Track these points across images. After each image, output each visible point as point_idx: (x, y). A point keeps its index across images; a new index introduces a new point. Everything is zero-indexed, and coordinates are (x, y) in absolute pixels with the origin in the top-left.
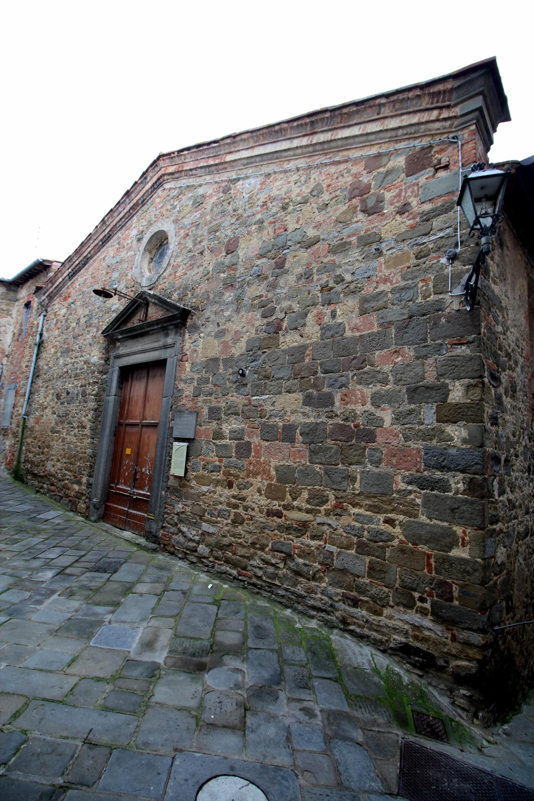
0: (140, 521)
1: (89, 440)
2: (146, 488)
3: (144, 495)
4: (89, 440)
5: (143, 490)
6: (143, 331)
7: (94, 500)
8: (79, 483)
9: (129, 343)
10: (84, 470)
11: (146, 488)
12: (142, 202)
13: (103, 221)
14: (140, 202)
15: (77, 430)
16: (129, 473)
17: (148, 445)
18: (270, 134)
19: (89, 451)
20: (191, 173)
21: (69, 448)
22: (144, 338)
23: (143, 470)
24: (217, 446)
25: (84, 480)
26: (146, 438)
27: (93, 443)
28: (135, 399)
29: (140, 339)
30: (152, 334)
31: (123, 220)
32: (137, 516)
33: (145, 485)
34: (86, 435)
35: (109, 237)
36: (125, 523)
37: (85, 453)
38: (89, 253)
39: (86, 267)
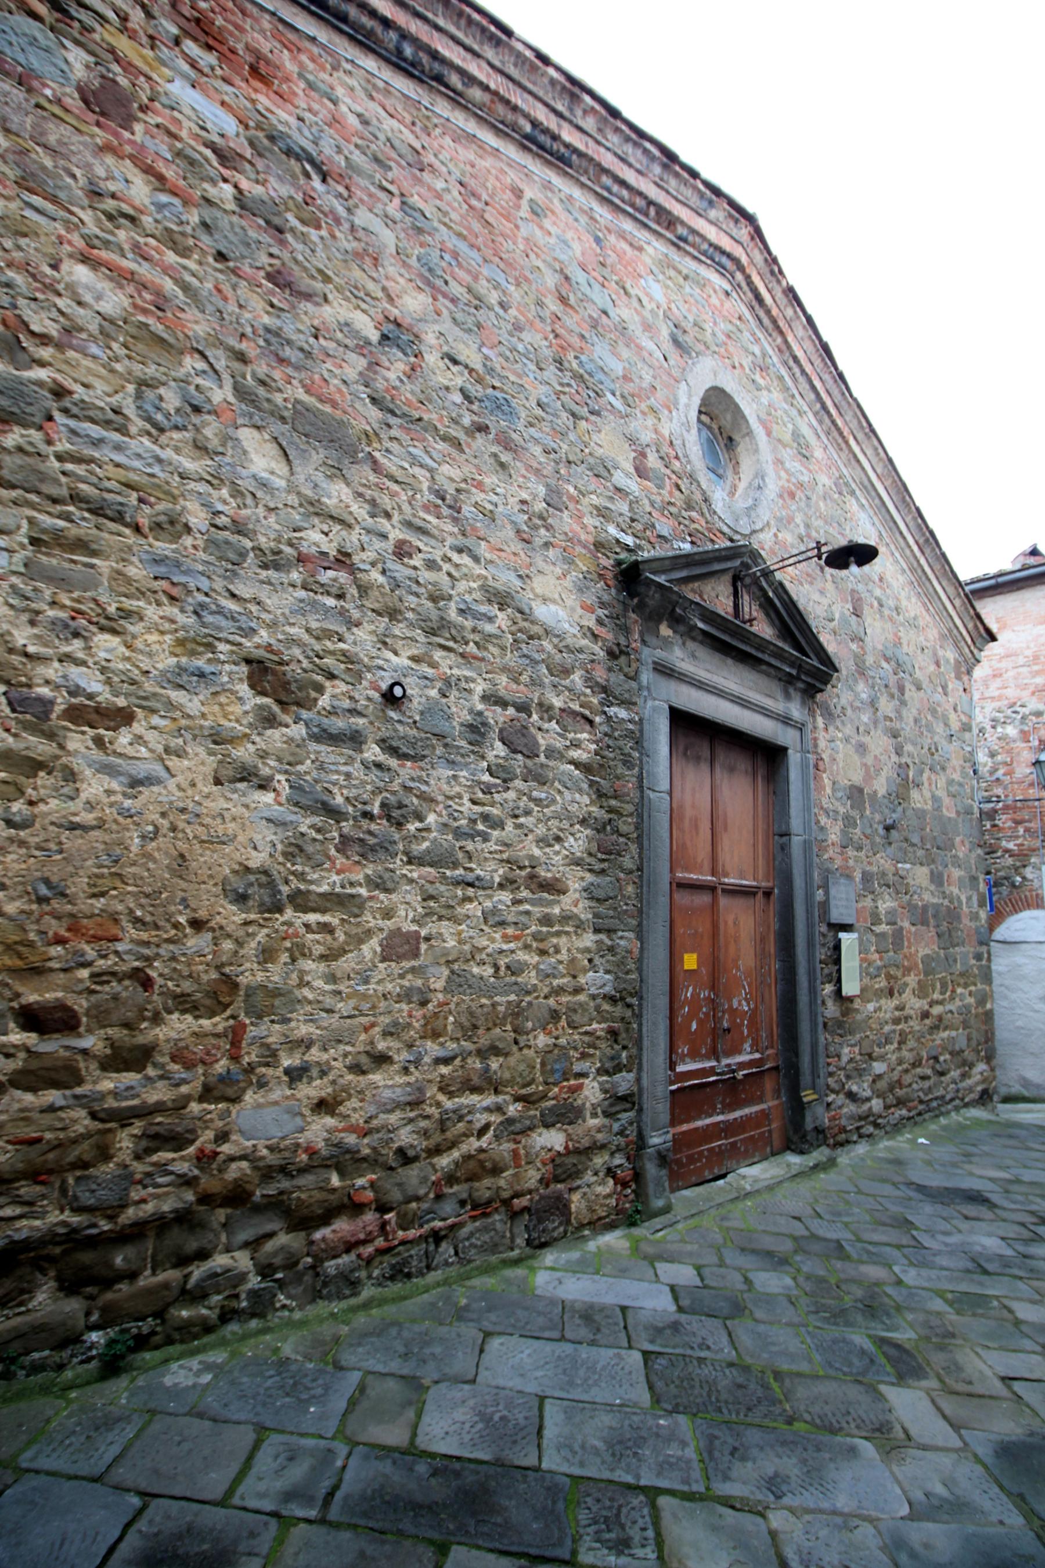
0: (757, 1127)
1: (589, 940)
2: (747, 1046)
3: (751, 1063)
4: (589, 940)
5: (740, 1052)
6: (760, 655)
7: (655, 1141)
8: (565, 1115)
9: (702, 652)
10: (584, 1056)
11: (747, 1046)
12: (680, 238)
13: (574, 88)
14: (681, 230)
15: (506, 896)
16: (700, 1023)
17: (737, 940)
18: (898, 492)
19: (597, 980)
20: (791, 363)
21: (458, 981)
22: (741, 666)
23: (735, 1004)
24: (877, 935)
25: (592, 1092)
26: (730, 923)
27: (611, 949)
28: (689, 813)
29: (730, 661)
30: (768, 675)
31: (625, 193)
32: (748, 1118)
33: (743, 1040)
34: (566, 918)
35: (561, 158)
36: (719, 1155)
37: (577, 991)
38: (470, 79)
39: (401, 84)
